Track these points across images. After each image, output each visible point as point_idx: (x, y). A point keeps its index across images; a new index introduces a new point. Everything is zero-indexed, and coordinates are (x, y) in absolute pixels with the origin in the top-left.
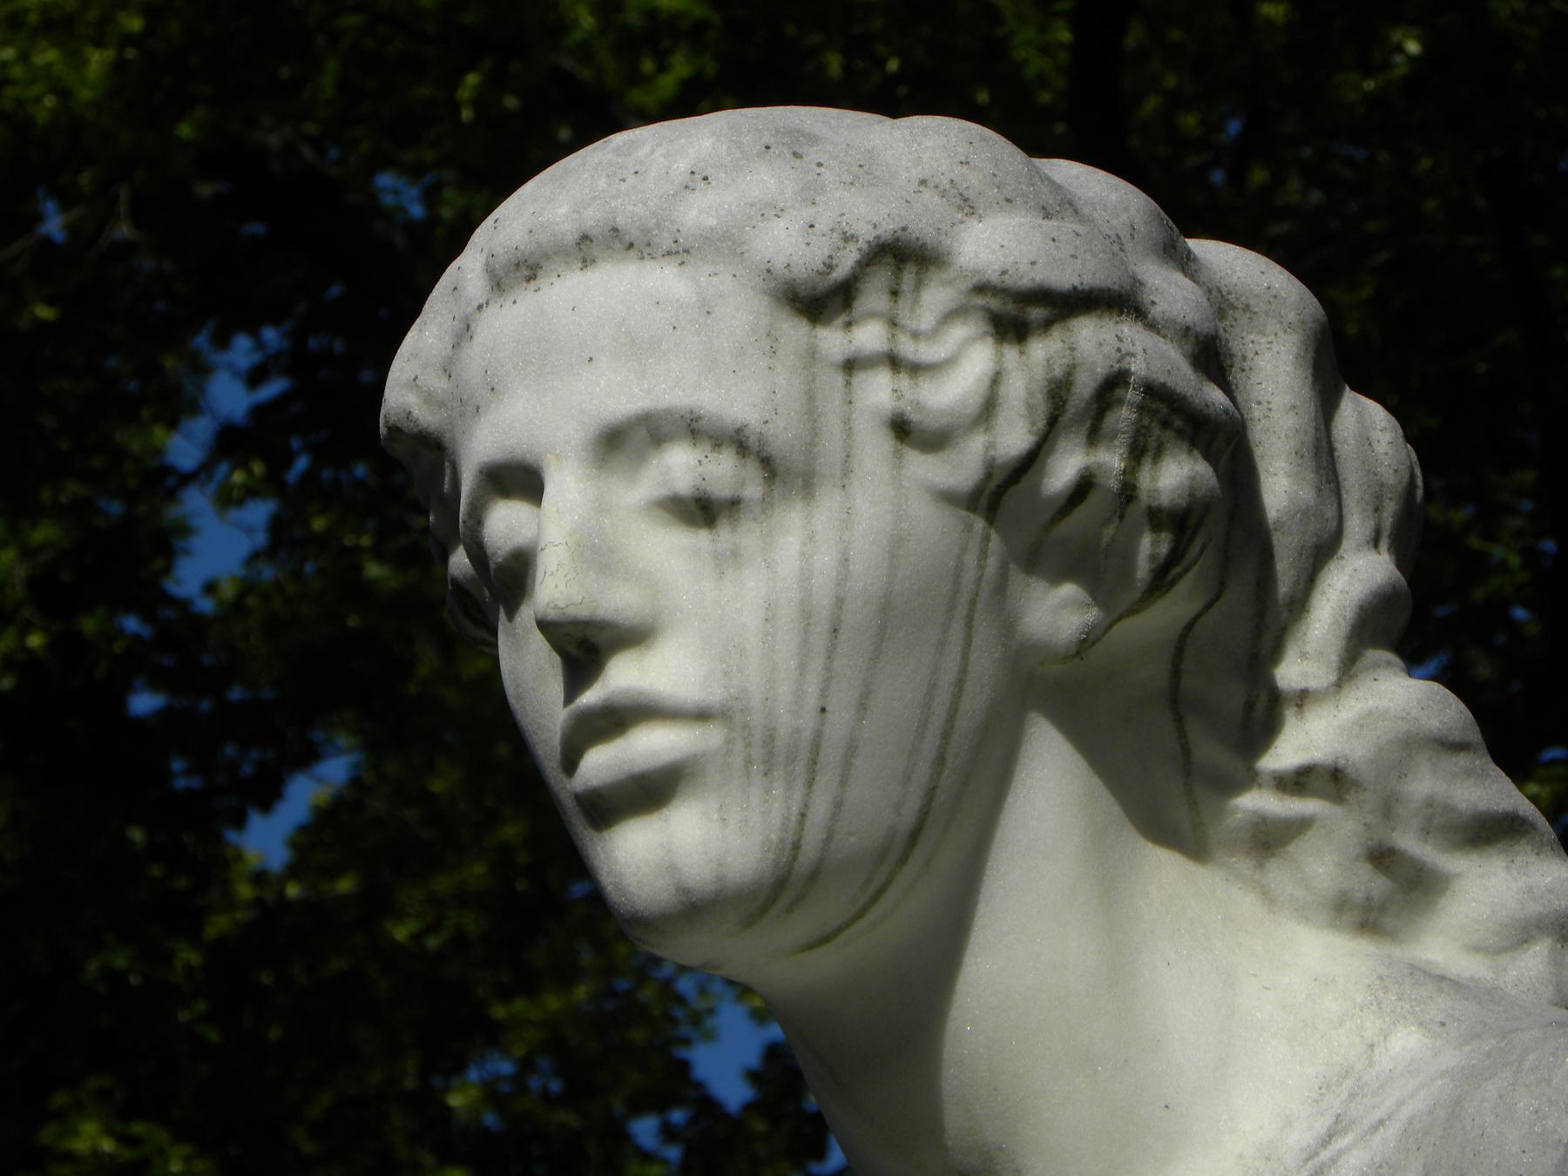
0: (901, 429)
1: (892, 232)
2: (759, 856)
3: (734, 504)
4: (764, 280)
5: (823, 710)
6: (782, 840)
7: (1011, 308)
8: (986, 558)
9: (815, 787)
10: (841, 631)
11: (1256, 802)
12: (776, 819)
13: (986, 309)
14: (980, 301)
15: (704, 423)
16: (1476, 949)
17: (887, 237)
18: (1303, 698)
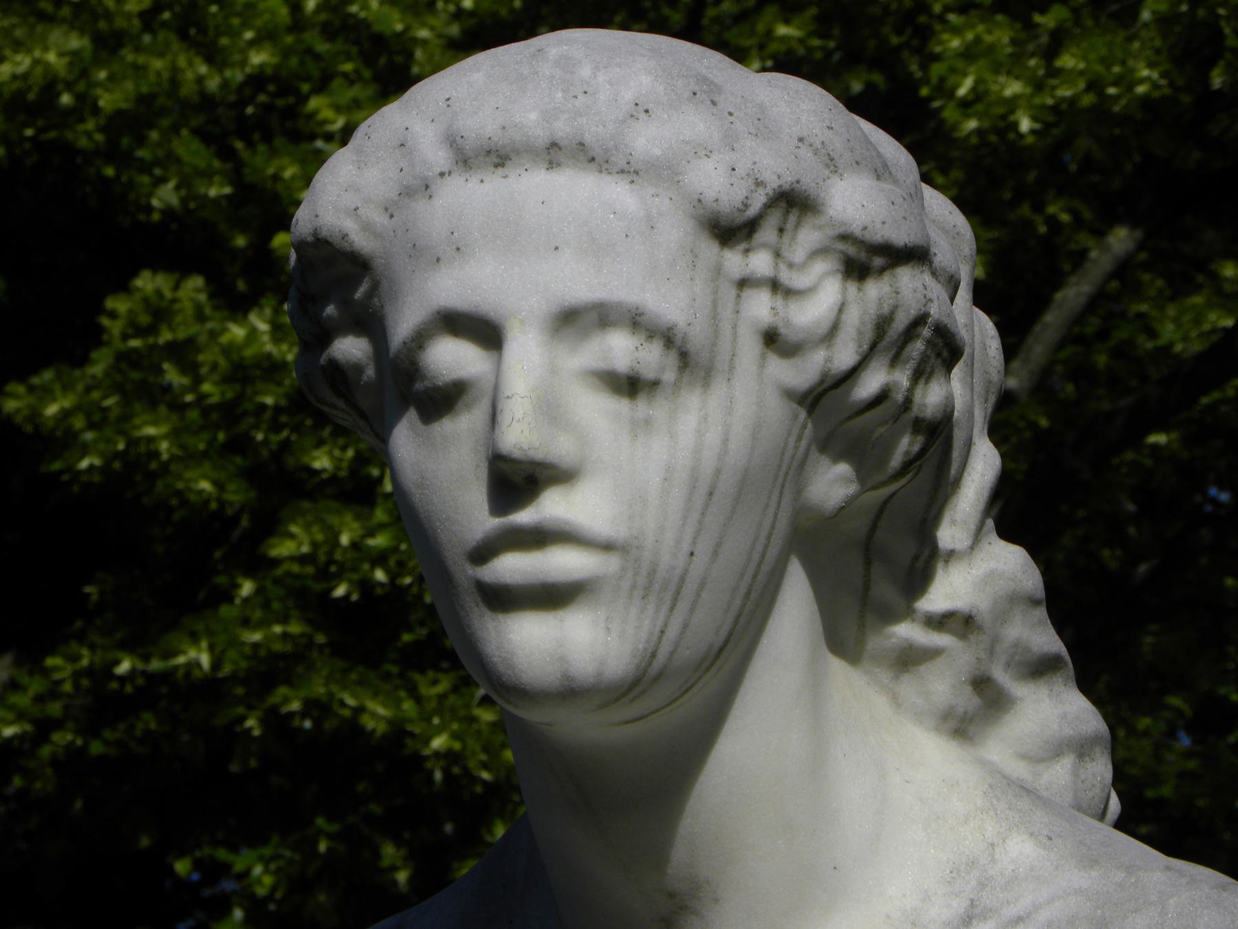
0: (771, 339)
1: (790, 184)
2: (628, 661)
3: (655, 384)
4: (694, 206)
5: (692, 554)
6: (645, 650)
7: (863, 255)
8: (800, 441)
9: (675, 611)
10: (714, 494)
11: (906, 631)
12: (644, 635)
13: (842, 252)
14: (841, 246)
15: (645, 318)
16: (1023, 756)
17: (786, 187)
18: (951, 555)
